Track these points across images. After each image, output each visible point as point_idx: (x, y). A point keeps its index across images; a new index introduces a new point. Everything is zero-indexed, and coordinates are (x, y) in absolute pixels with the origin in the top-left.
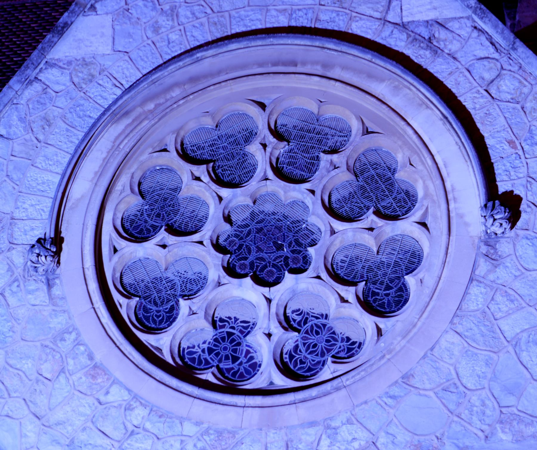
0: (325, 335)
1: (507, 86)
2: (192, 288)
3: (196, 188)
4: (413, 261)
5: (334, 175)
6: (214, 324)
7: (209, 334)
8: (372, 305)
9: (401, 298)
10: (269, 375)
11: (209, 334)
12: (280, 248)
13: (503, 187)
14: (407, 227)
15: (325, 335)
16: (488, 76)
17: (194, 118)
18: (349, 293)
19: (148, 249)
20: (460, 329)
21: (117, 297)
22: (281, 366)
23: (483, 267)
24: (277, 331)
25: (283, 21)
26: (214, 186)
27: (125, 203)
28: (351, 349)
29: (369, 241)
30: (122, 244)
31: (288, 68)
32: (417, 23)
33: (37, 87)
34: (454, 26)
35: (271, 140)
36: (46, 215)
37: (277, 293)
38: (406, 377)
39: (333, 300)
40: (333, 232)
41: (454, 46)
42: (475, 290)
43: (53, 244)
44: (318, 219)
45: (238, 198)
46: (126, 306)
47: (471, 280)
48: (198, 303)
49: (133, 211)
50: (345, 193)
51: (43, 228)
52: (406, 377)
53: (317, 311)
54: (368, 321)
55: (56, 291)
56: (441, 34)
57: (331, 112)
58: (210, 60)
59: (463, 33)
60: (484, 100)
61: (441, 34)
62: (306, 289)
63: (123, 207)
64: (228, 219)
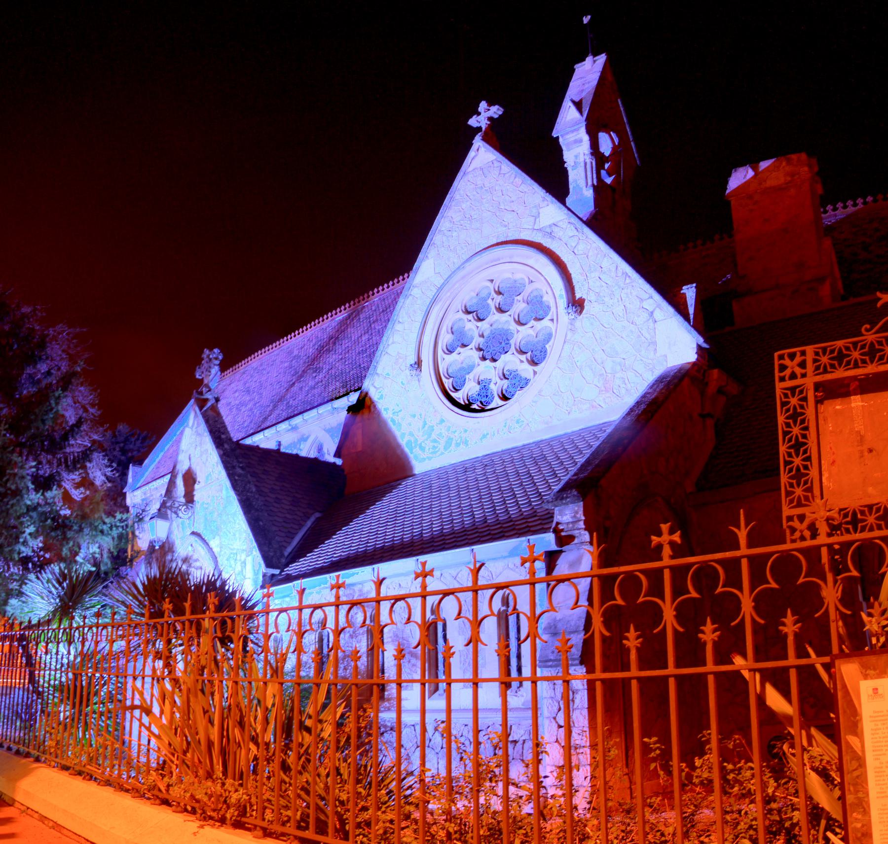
0: (518, 379)
1: (581, 247)
2: (470, 369)
3: (471, 326)
4: (549, 337)
5: (519, 307)
6: (479, 383)
7: (478, 388)
8: (533, 362)
9: (544, 353)
10: (497, 401)
11: (478, 388)
12: (501, 343)
13: (578, 296)
14: (546, 322)
15: (518, 379)
16: (574, 245)
17: (467, 295)
18: (523, 358)
19: (454, 355)
20: (560, 366)
21: (444, 380)
22: (141, 590)
23: (570, 334)
24: (499, 381)
25: (495, 242)
26: (475, 323)
27: (446, 338)
28: (527, 381)
29: (532, 332)
30: (445, 356)
31: (496, 263)
32: (545, 227)
33: (411, 298)
34: (560, 224)
35: (495, 296)
36: (413, 353)
37: (498, 364)
38: (540, 391)
39: (518, 362)
40: (518, 331)
41: (561, 234)
42: (567, 346)
43: (418, 364)
44: (513, 327)
45: (484, 326)
46: (448, 384)
47: (565, 342)
48: (471, 376)
49: (451, 341)
50: (525, 312)
51: (412, 359)
52: (540, 391)
53: (515, 369)
54: (531, 368)
55: (421, 383)
56: (555, 229)
57: (518, 276)
58: (469, 267)
59: (564, 226)
60: (572, 256)
61: (555, 229)
62: (511, 361)
63: (445, 341)
64: (482, 336)
